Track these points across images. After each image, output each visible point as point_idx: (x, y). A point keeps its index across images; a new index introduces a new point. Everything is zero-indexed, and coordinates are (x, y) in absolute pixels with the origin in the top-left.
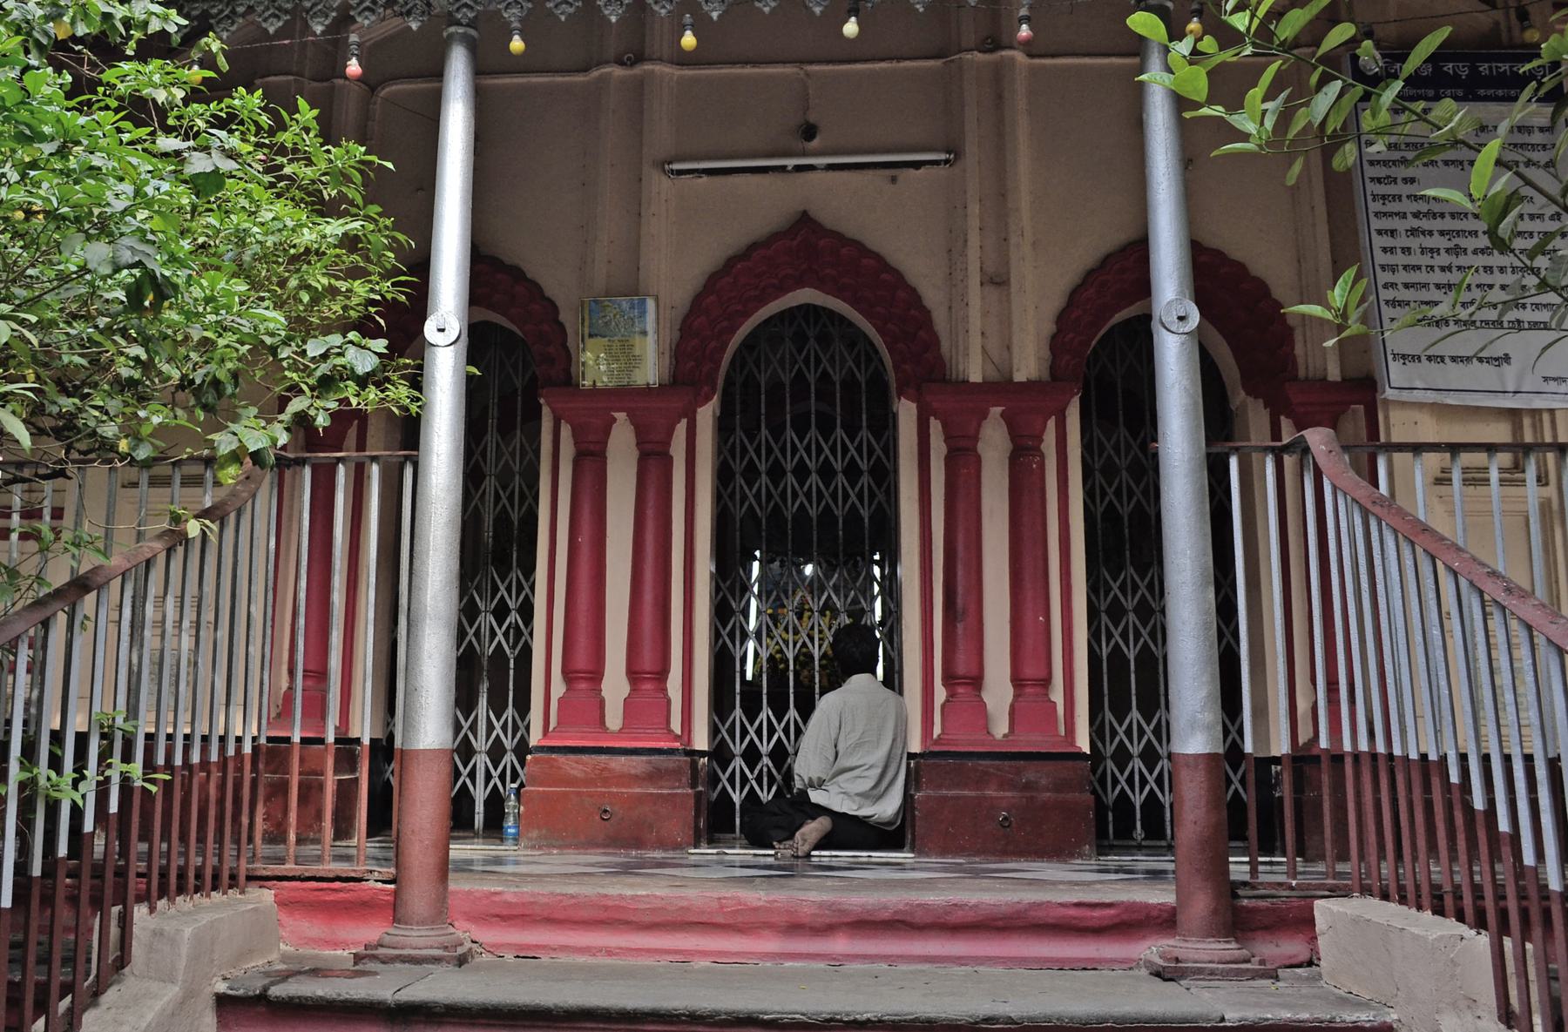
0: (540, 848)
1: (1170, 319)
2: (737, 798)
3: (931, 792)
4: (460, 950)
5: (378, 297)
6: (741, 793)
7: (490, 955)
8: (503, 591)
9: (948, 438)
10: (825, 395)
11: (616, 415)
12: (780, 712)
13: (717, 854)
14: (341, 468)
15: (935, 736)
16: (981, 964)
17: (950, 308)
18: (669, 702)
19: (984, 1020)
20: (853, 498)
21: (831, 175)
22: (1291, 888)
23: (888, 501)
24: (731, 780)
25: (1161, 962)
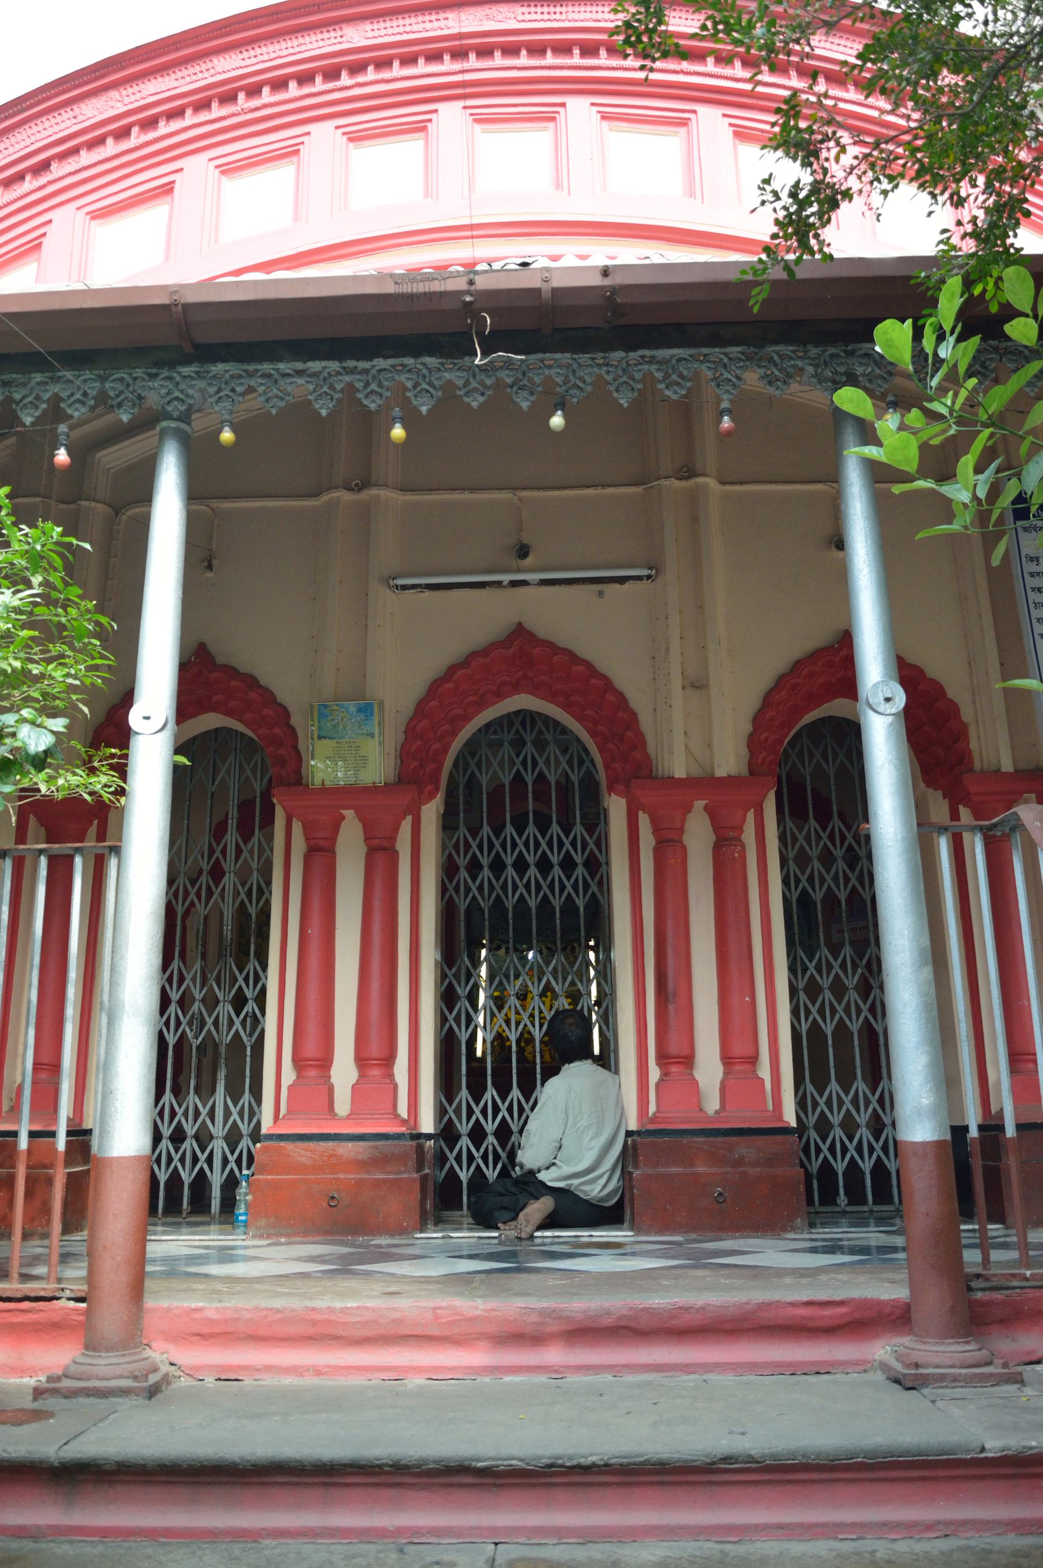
0: (268, 1237)
1: (877, 700)
2: (464, 1176)
3: (648, 1170)
4: (153, 1379)
5: (77, 682)
6: (468, 1171)
7: (189, 1379)
8: (241, 981)
9: (656, 830)
10: (543, 795)
11: (344, 812)
12: (504, 1093)
13: (443, 1238)
14: (78, 861)
15: (650, 1114)
16: (711, 1372)
17: (655, 710)
18: (395, 1087)
19: (721, 1459)
20: (569, 889)
21: (544, 589)
22: (1026, 1279)
23: (601, 892)
24: (458, 1159)
25: (898, 1367)
